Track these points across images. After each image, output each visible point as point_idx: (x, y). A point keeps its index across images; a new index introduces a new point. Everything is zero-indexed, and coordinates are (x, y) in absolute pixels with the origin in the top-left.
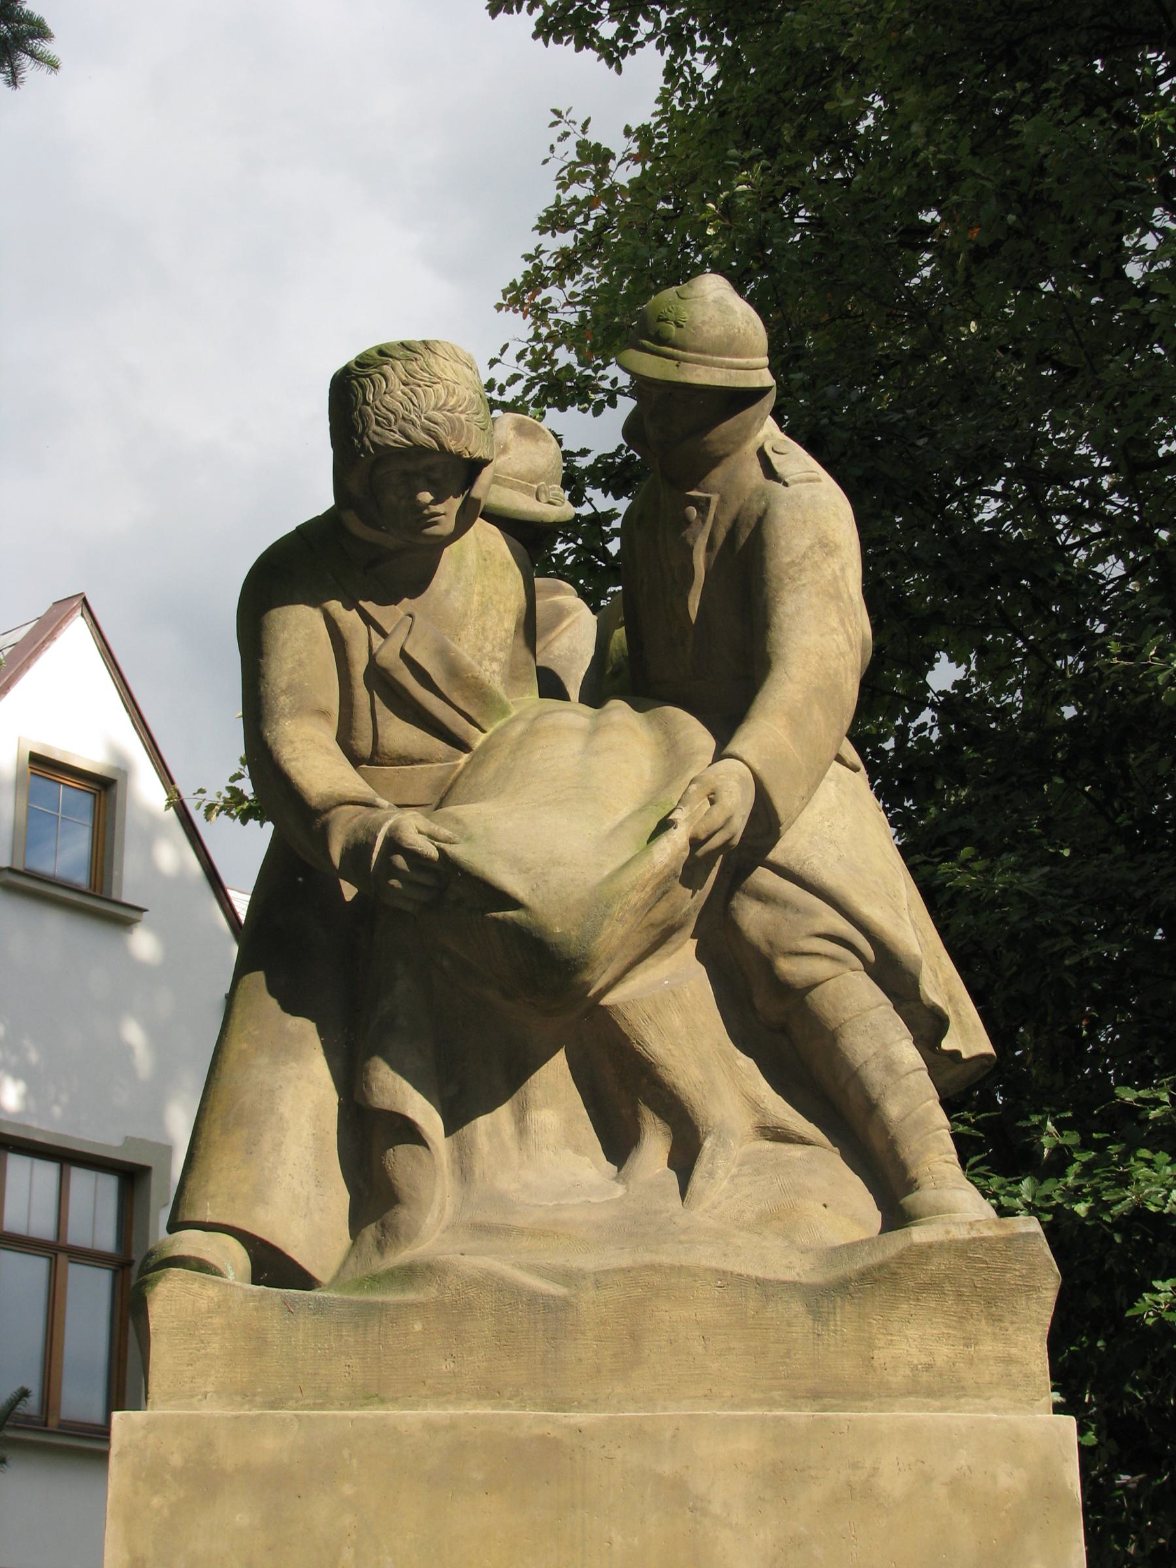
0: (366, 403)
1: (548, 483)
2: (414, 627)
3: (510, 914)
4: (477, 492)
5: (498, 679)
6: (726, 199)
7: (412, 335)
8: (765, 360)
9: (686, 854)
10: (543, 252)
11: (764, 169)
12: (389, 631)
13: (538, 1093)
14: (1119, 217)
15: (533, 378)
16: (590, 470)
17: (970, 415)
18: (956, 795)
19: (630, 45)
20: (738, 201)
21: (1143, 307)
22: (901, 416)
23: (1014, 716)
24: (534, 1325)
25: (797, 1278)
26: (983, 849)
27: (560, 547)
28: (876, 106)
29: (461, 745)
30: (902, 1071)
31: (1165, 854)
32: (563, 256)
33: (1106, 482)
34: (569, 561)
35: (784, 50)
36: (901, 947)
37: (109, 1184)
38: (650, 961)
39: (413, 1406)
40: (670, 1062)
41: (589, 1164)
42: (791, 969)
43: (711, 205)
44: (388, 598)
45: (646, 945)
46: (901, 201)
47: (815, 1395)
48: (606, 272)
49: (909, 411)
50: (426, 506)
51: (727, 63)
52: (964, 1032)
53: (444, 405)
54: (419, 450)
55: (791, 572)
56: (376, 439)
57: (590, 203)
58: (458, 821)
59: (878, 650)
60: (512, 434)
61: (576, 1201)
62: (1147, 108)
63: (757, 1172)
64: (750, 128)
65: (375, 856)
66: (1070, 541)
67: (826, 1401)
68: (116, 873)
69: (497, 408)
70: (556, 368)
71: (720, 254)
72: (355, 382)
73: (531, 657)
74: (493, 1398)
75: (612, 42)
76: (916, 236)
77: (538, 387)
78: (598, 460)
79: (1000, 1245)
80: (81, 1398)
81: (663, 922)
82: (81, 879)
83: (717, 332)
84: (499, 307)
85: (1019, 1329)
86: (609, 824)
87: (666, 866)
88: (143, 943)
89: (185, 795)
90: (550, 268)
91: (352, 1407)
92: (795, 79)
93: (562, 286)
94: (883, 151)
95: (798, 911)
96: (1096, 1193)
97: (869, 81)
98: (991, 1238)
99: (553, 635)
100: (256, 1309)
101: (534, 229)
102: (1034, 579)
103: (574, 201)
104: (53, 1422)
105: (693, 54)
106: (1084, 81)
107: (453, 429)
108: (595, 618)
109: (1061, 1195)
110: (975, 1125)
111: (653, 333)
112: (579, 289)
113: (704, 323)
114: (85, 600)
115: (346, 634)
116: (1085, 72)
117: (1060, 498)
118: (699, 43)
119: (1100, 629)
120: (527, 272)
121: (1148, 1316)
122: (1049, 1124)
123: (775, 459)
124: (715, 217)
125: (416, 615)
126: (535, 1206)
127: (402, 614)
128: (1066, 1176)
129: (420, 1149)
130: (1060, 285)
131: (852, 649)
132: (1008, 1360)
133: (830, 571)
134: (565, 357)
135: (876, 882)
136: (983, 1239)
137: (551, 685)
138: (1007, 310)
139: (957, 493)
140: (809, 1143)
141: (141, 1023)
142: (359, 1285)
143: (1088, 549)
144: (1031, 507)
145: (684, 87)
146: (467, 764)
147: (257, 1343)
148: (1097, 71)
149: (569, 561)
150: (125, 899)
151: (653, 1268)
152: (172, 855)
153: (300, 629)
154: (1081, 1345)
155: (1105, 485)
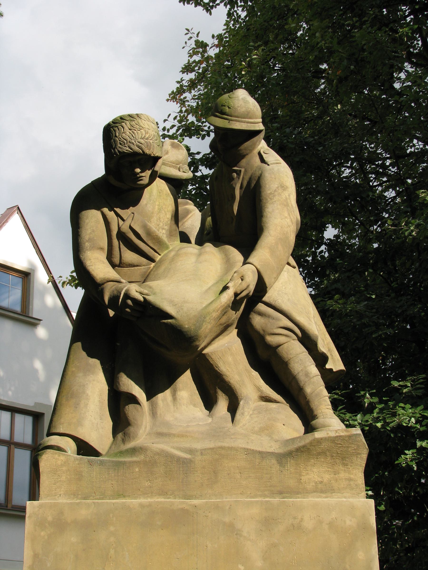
0: (116, 136)
1: (183, 165)
2: (134, 218)
3: (169, 321)
4: (157, 168)
5: (165, 236)
6: (249, 61)
7: (133, 112)
8: (261, 120)
9: (233, 299)
10: (184, 80)
11: (263, 50)
12: (125, 219)
13: (180, 385)
14: (392, 66)
15: (179, 126)
16: (201, 159)
17: (338, 139)
18: (334, 276)
19: (214, 5)
20: (254, 61)
21: (399, 99)
22: (312, 139)
23: (355, 247)
24: (179, 468)
25: (274, 451)
26: (344, 295)
27: (190, 187)
28: (303, 26)
29: (152, 260)
30: (312, 376)
31: (409, 297)
32: (191, 82)
33: (388, 162)
34: (193, 193)
35: (270, 6)
36: (310, 331)
37: (29, 420)
38: (220, 337)
39: (135, 498)
40: (228, 373)
41: (199, 410)
42: (271, 340)
43: (243, 63)
44: (125, 207)
45: (219, 332)
46: (313, 61)
47: (280, 493)
48: (206, 87)
49: (316, 137)
50: (138, 174)
51: (250, 11)
52: (334, 361)
53: (144, 137)
54: (135, 154)
55: (270, 196)
56: (120, 150)
57: (200, 62)
58: (150, 287)
59: (303, 223)
60: (170, 147)
61: (195, 424)
62: (402, 27)
63: (259, 413)
64: (258, 35)
65: (120, 300)
66: (375, 184)
67: (284, 495)
68: (31, 307)
69: (167, 137)
70: (188, 123)
71: (247, 81)
72: (112, 129)
73: (177, 228)
74: (164, 495)
75: (208, 4)
76: (319, 74)
77: (181, 130)
78: (204, 155)
79: (347, 439)
80: (19, 496)
81: (225, 323)
82: (18, 309)
83: (243, 110)
84: (168, 100)
85: (354, 468)
86: (205, 288)
87: (226, 303)
88: (41, 332)
89: (56, 278)
90: (186, 86)
91: (113, 499)
92: (274, 17)
93: (190, 92)
94: (306, 43)
95: (274, 319)
96: (384, 419)
97: (301, 18)
98: (343, 436)
99: (185, 220)
100: (79, 464)
101: (180, 72)
102: (361, 198)
103: (194, 61)
104: (9, 506)
105: (237, 8)
106: (379, 17)
107: (148, 146)
108: (200, 213)
109: (372, 420)
110: (341, 395)
111: (220, 111)
112: (196, 94)
113: (238, 107)
114: (18, 208)
115: (110, 220)
116: (379, 14)
117: (372, 168)
118: (239, 4)
119: (387, 216)
120: (178, 87)
121: (403, 463)
122: (367, 394)
123: (264, 156)
124: (246, 67)
125: (135, 213)
126: (179, 426)
127: (130, 212)
128: (373, 413)
129: (138, 406)
130: (370, 91)
131: (292, 224)
132: (350, 480)
133: (284, 196)
134: (191, 118)
135: (302, 308)
136: (340, 436)
137: (184, 238)
138: (352, 100)
139: (334, 167)
140: (278, 402)
141: (38, 360)
142: (116, 455)
143: (382, 187)
144: (361, 171)
145: (234, 20)
146: (154, 267)
147: (79, 476)
148: (384, 13)
149: (193, 193)
150: (34, 316)
151: (222, 448)
152: (51, 300)
153: (93, 219)
154: (379, 474)
155: (388, 164)
